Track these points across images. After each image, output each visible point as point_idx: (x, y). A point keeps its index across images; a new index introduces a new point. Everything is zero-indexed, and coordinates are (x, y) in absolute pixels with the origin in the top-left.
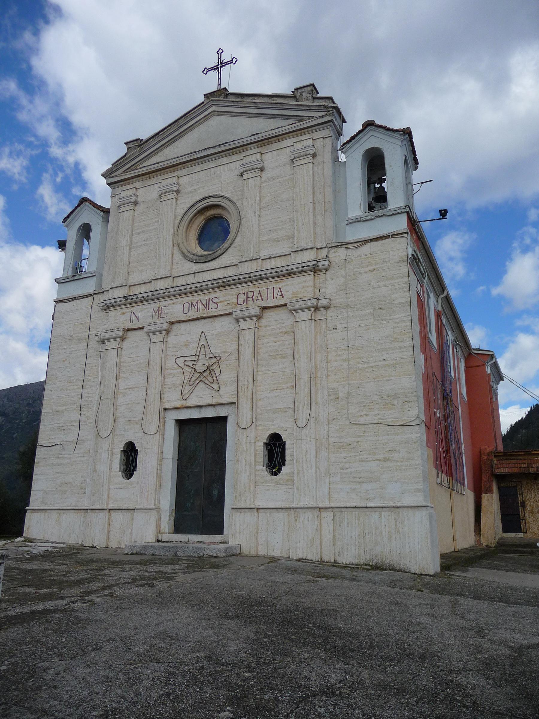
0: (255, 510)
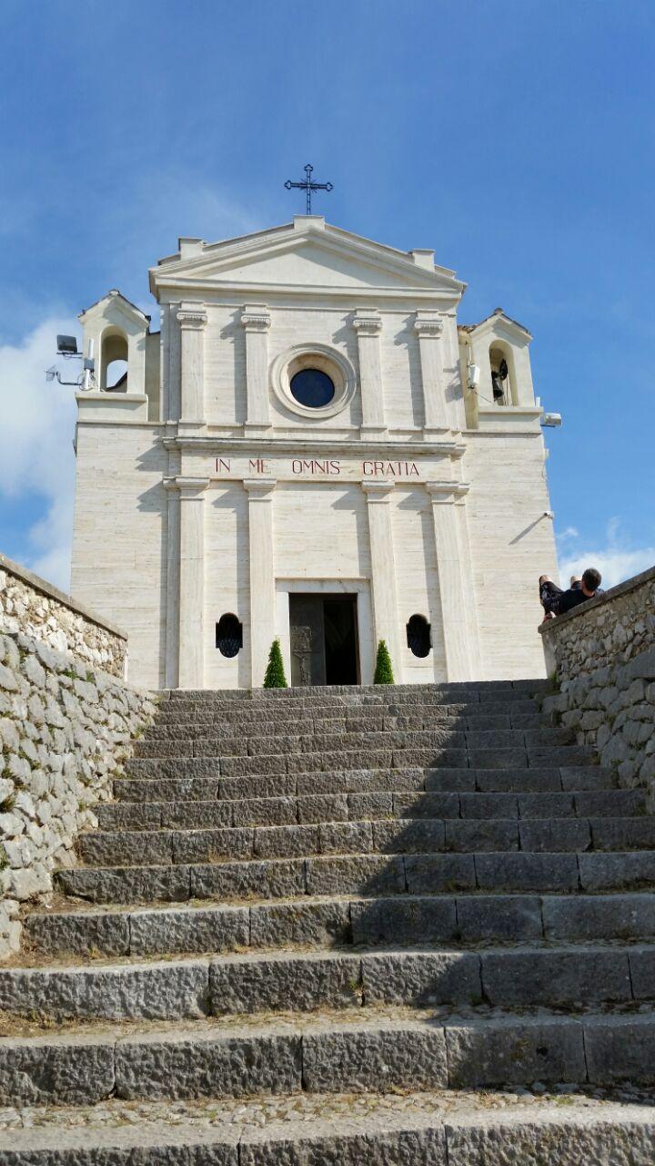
0: (434, 566)
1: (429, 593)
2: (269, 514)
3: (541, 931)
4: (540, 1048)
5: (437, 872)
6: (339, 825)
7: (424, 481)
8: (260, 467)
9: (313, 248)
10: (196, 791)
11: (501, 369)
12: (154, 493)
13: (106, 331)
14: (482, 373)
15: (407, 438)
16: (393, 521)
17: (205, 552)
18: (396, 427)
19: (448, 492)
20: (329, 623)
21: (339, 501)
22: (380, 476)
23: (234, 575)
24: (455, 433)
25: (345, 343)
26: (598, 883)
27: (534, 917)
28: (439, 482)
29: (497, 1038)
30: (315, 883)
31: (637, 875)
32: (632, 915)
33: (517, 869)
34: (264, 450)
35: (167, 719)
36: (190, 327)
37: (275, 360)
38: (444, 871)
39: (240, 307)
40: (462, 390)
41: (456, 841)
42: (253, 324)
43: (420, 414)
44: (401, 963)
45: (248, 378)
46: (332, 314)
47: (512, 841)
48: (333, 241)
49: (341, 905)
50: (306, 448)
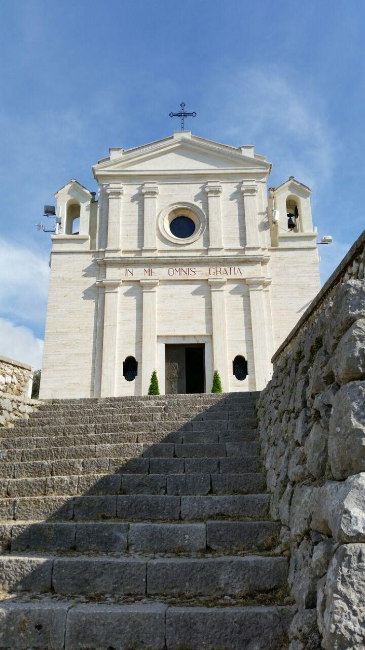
1: (246, 343)
2: (154, 300)
3: (126, 546)
4: (38, 624)
5: (93, 507)
6: (58, 478)
7: (245, 278)
8: (150, 273)
9: (184, 149)
10: (9, 457)
11: (293, 211)
12: (91, 290)
13: (69, 202)
14: (280, 214)
15: (235, 253)
16: (226, 302)
17: (118, 321)
18: (229, 247)
19: (259, 283)
20: (188, 360)
21: (195, 291)
22: (219, 275)
23: (134, 334)
24: (264, 249)
25: (201, 201)
26: (192, 516)
27: (122, 537)
28: (253, 278)
29: (12, 617)
30: (19, 512)
31: (217, 511)
32: (185, 538)
33: (142, 505)
34: (152, 263)
35: (36, 415)
36: (114, 197)
37: (160, 213)
38: (98, 507)
39: (142, 184)
40: (269, 225)
41: (128, 488)
42: (148, 193)
43: (243, 239)
44: (5, 564)
45: (145, 223)
46: (193, 185)
47: (161, 488)
48: (195, 144)
49: (7, 527)
50: (177, 261)
